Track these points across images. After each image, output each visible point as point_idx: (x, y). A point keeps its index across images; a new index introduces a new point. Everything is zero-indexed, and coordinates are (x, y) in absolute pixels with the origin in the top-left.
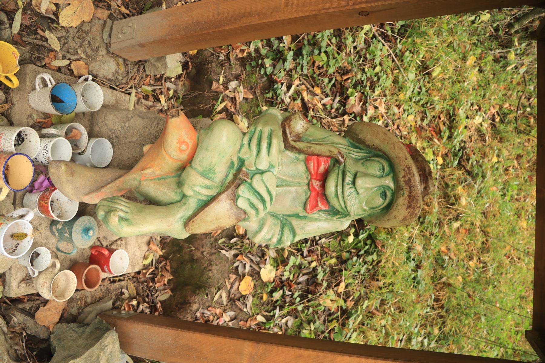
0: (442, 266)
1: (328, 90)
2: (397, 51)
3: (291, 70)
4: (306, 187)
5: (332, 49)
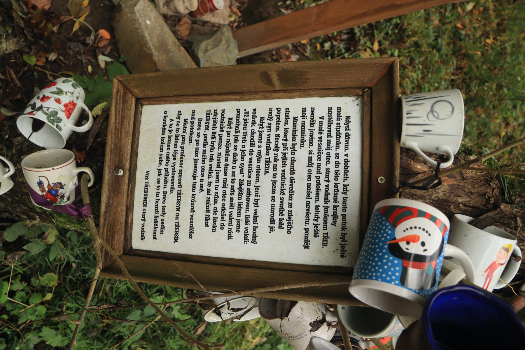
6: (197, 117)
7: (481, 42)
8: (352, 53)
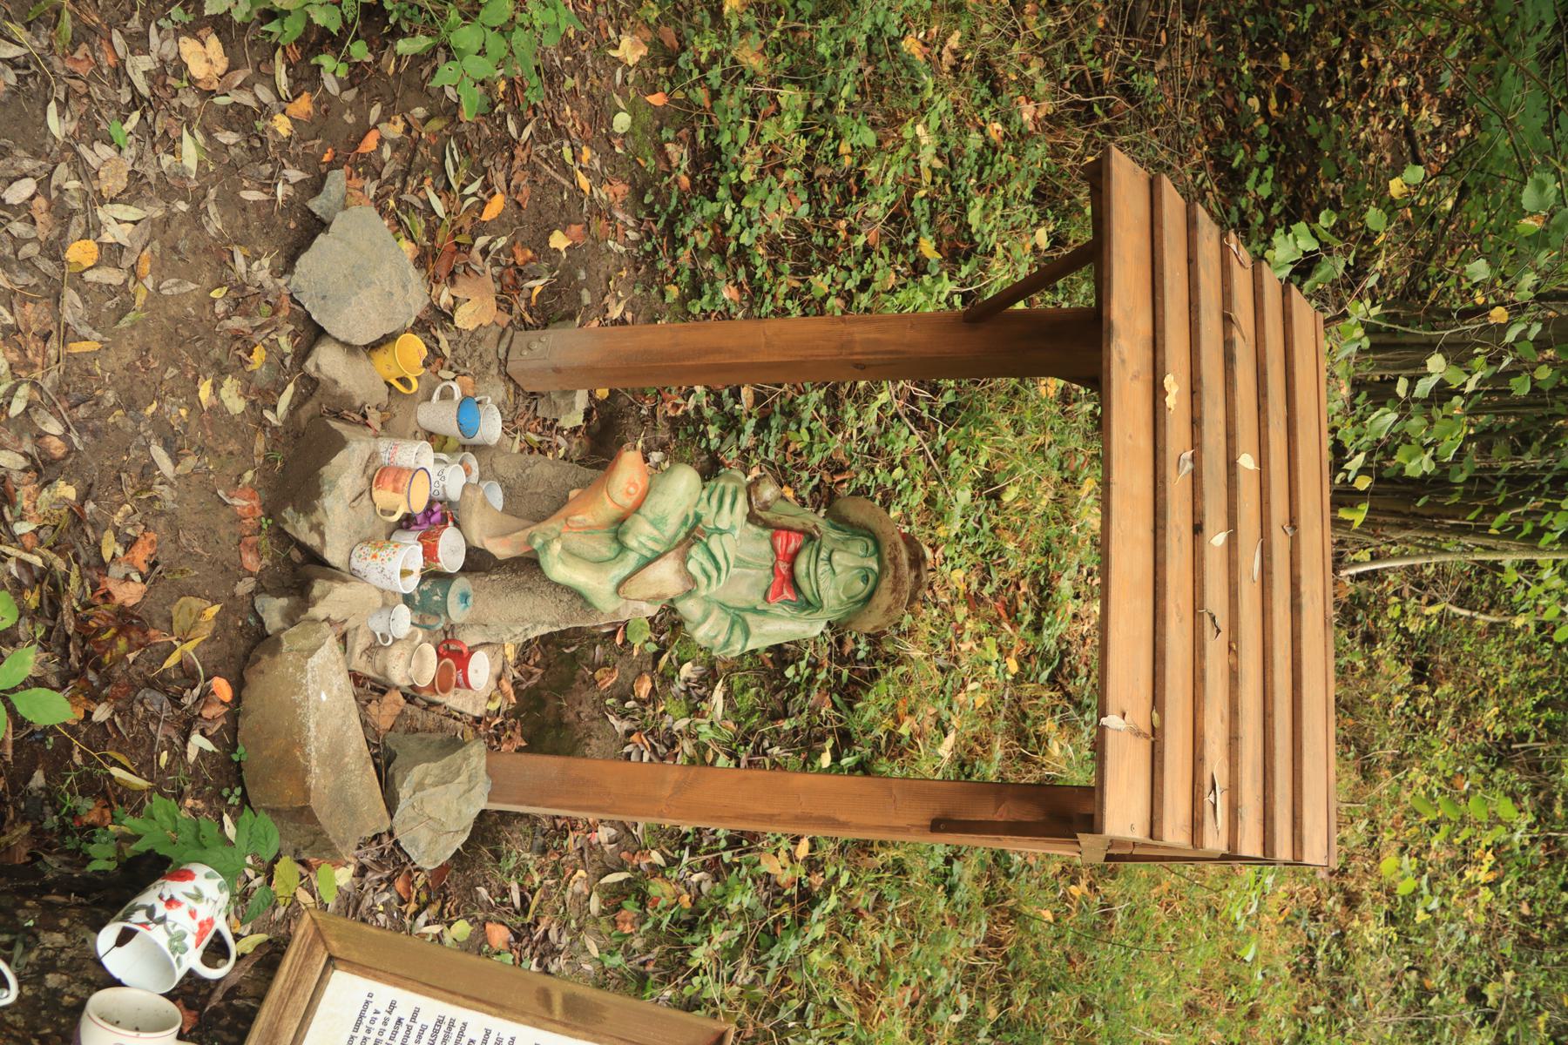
0: (1007, 869)
1: (805, 494)
2: (938, 447)
3: (748, 450)
4: (769, 572)
5: (821, 426)
6: (420, 1020)
7: (1056, 890)
8: (740, 853)
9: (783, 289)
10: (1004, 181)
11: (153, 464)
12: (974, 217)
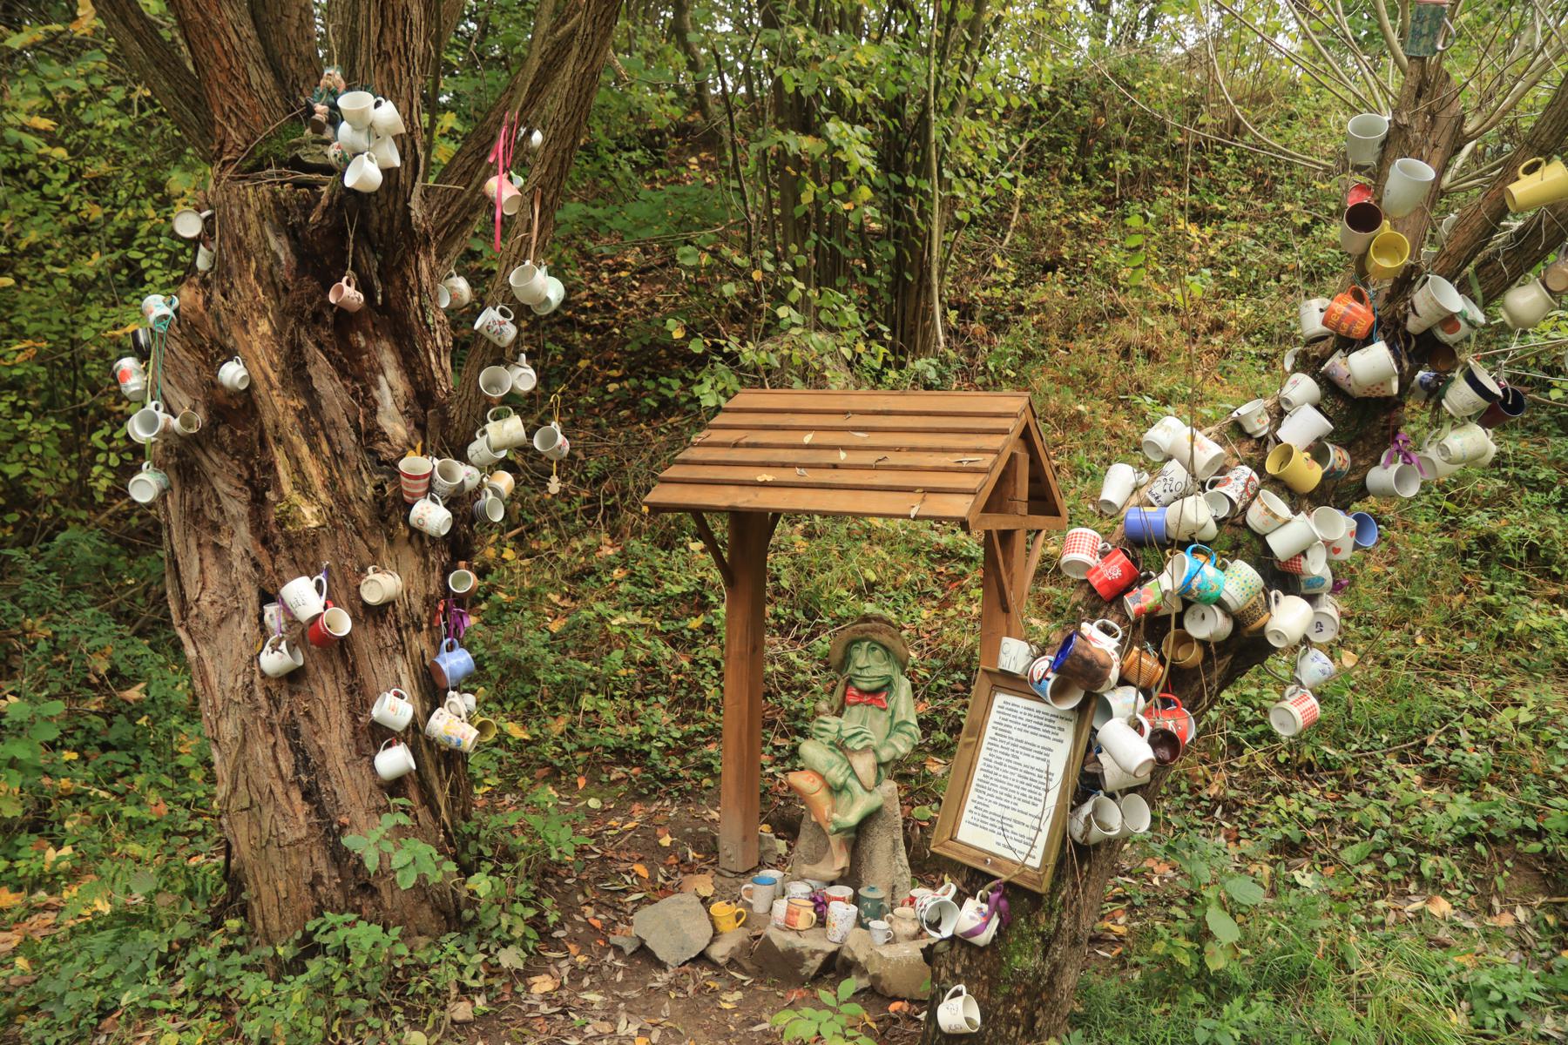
9: (713, 716)
10: (654, 570)
11: (763, 1032)
12: (677, 590)
